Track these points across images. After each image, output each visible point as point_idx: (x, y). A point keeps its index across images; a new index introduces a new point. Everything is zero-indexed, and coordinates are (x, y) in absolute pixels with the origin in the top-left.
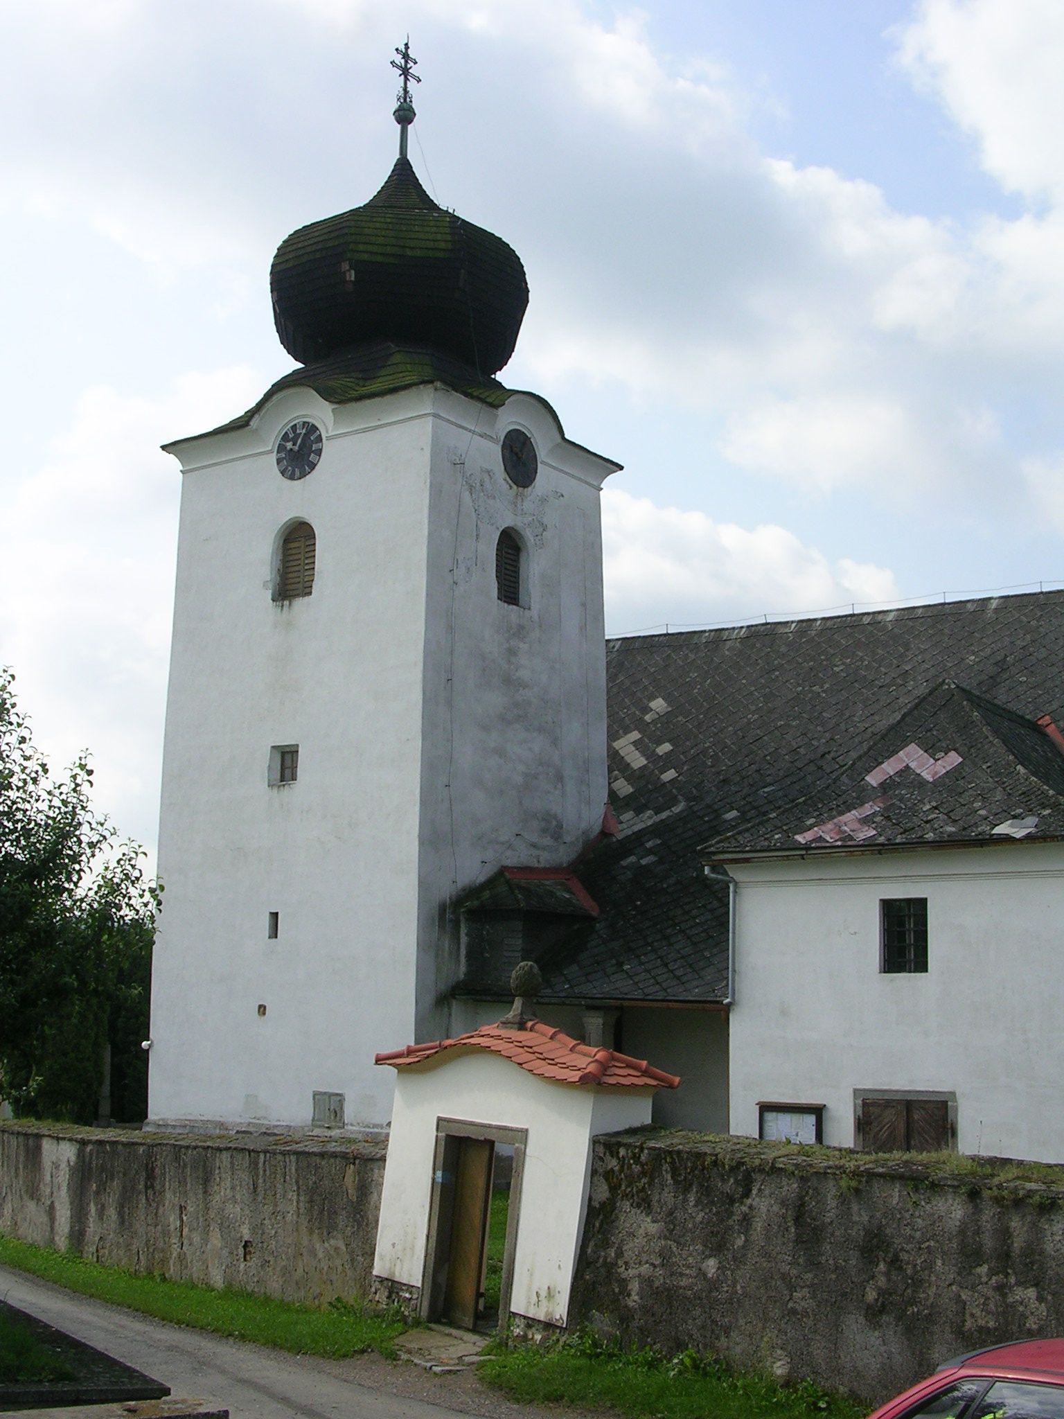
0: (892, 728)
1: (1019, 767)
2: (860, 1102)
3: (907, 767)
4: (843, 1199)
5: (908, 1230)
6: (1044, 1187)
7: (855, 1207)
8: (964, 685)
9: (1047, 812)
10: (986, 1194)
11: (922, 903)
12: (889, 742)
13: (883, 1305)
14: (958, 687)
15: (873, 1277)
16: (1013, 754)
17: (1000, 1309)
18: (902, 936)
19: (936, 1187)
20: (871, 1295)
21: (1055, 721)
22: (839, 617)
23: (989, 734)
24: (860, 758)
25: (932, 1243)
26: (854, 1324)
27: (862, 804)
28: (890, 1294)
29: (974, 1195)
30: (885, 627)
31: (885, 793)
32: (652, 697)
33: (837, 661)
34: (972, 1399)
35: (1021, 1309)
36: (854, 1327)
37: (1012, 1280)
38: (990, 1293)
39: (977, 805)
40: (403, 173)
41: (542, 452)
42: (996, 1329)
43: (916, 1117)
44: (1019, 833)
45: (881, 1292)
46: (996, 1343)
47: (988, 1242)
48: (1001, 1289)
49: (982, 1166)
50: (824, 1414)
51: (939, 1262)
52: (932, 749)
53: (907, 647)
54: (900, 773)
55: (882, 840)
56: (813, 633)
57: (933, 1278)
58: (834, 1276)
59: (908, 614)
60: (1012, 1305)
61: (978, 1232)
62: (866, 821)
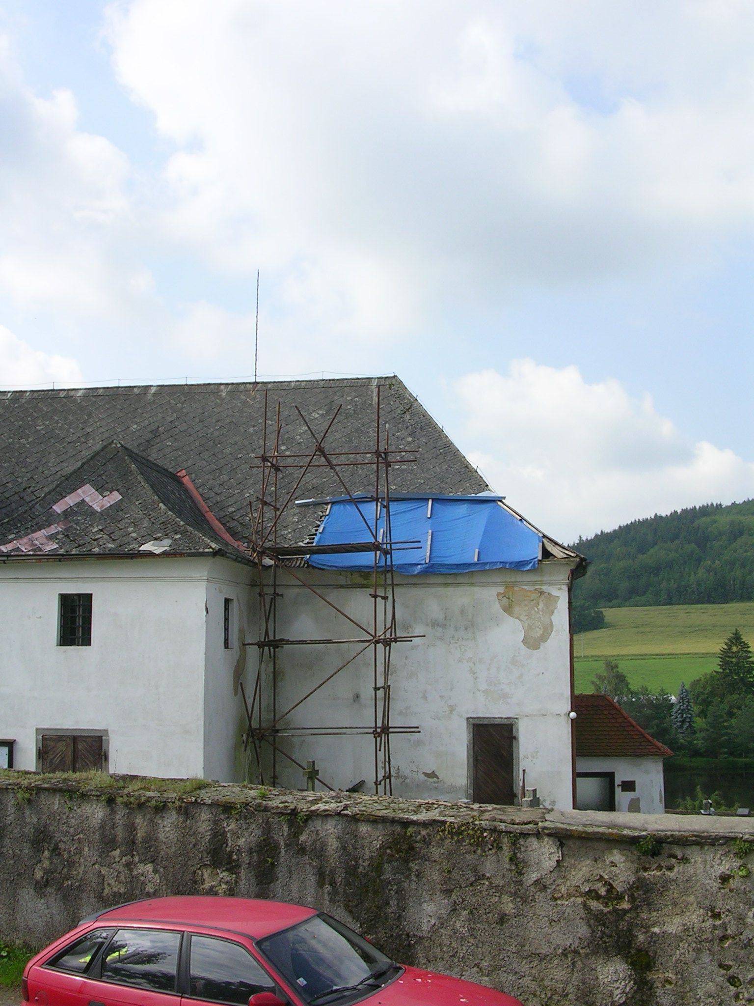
0: (75, 472)
1: (161, 505)
2: (40, 737)
3: (83, 501)
4: (19, 807)
5: (65, 828)
6: (158, 794)
7: (28, 812)
8: (128, 446)
9: (179, 536)
10: (119, 800)
11: (89, 597)
12: (71, 483)
13: (47, 881)
14: (122, 446)
15: (40, 861)
16: (158, 495)
17: (128, 880)
18: (73, 620)
19: (84, 796)
20: (39, 874)
21: (189, 474)
22: (43, 391)
23: (142, 480)
24: (49, 493)
25: (81, 836)
26: (27, 895)
27: (49, 526)
28: (52, 873)
29: (111, 801)
30: (75, 400)
31: (66, 518)
33: (39, 422)
34: (102, 943)
35: (142, 878)
36: (27, 897)
37: (136, 859)
38: (121, 869)
39: (130, 529)
42: (125, 893)
43: (80, 747)
44: (158, 550)
45: (46, 872)
46: (115, 905)
47: (120, 834)
48: (128, 865)
49: (117, 781)
50: (6, 960)
51: (86, 849)
52: (101, 489)
53: (90, 415)
54: (77, 505)
55: (62, 551)
56: (24, 401)
57: (82, 860)
58: (12, 862)
59: (92, 393)
60: (137, 877)
61: (113, 827)
62: (51, 538)
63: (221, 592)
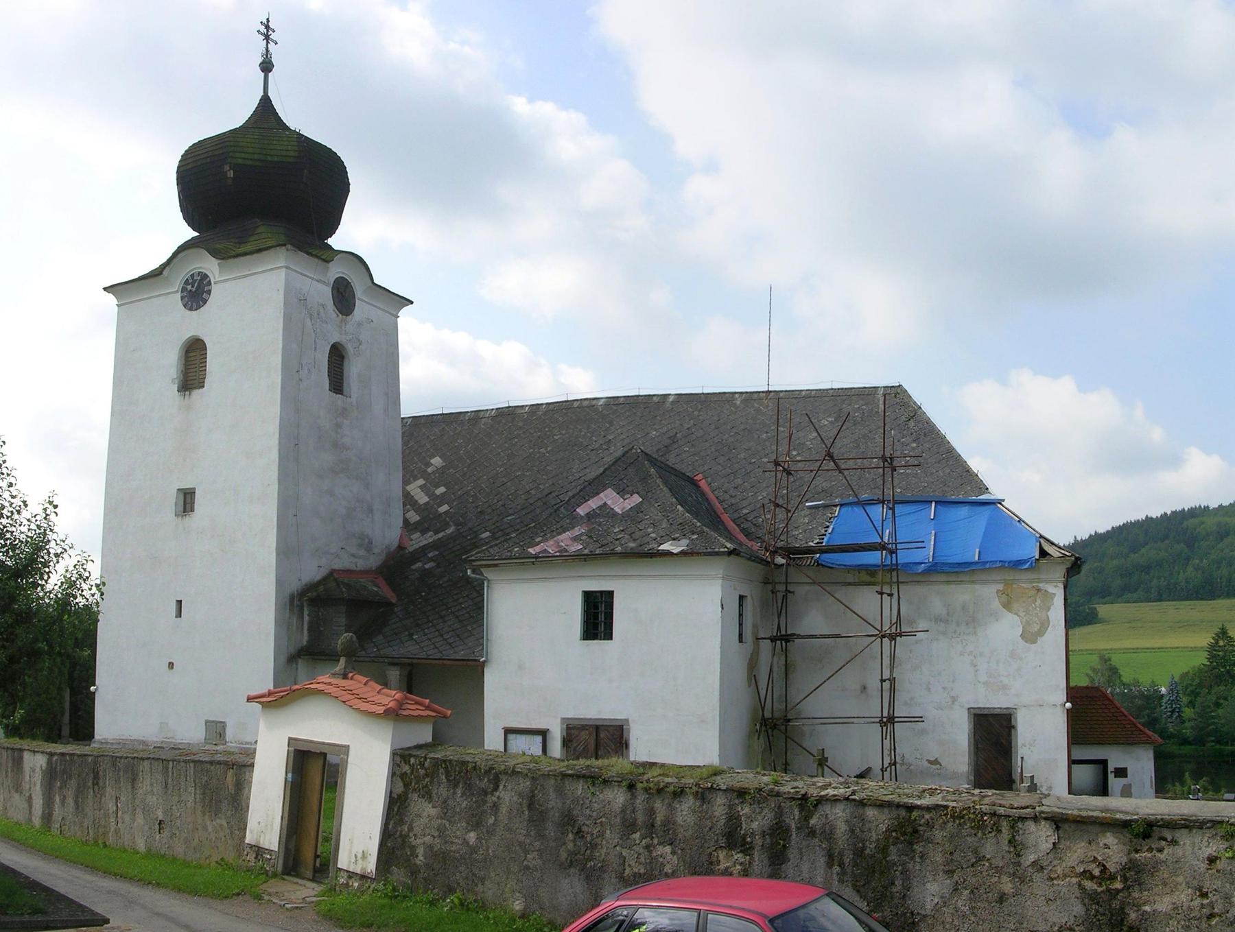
32: (433, 456)
40: (266, 105)
41: (359, 293)
44: (676, 550)
62: (576, 539)
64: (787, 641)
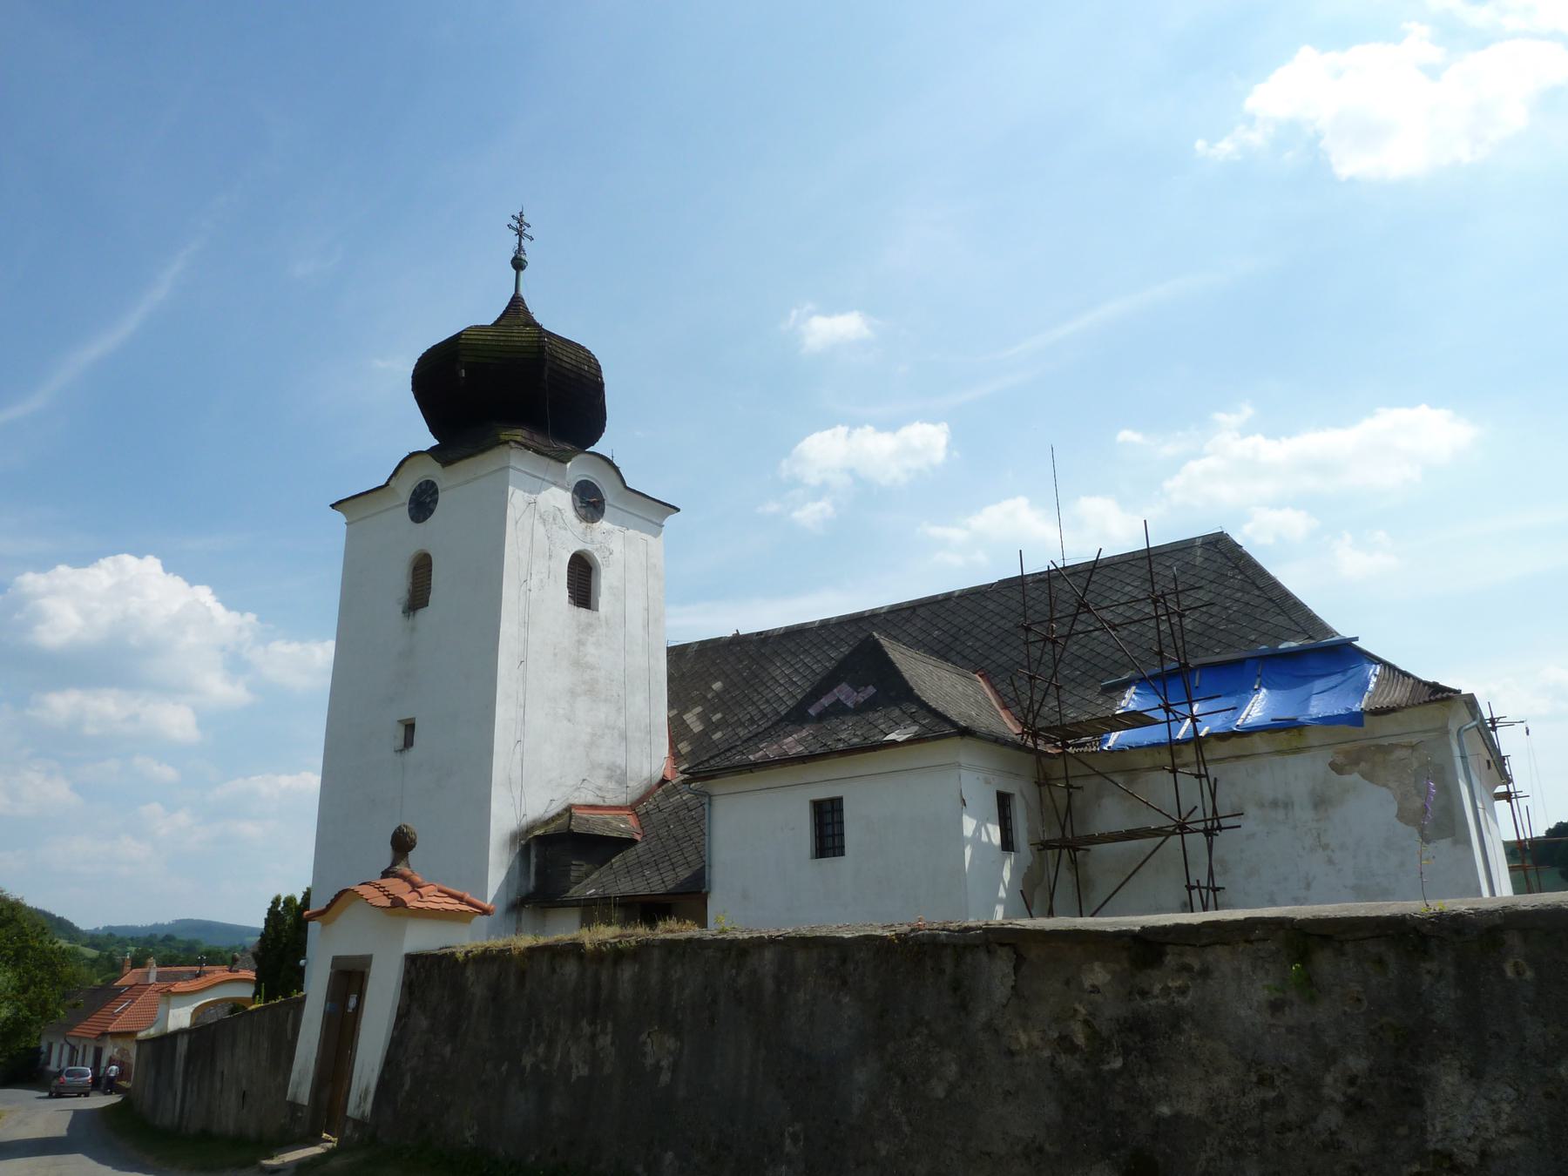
11: (840, 800)
32: (716, 679)
40: (516, 304)
41: (609, 497)
44: (901, 738)
62: (799, 742)
63: (987, 782)
64: (1076, 850)
